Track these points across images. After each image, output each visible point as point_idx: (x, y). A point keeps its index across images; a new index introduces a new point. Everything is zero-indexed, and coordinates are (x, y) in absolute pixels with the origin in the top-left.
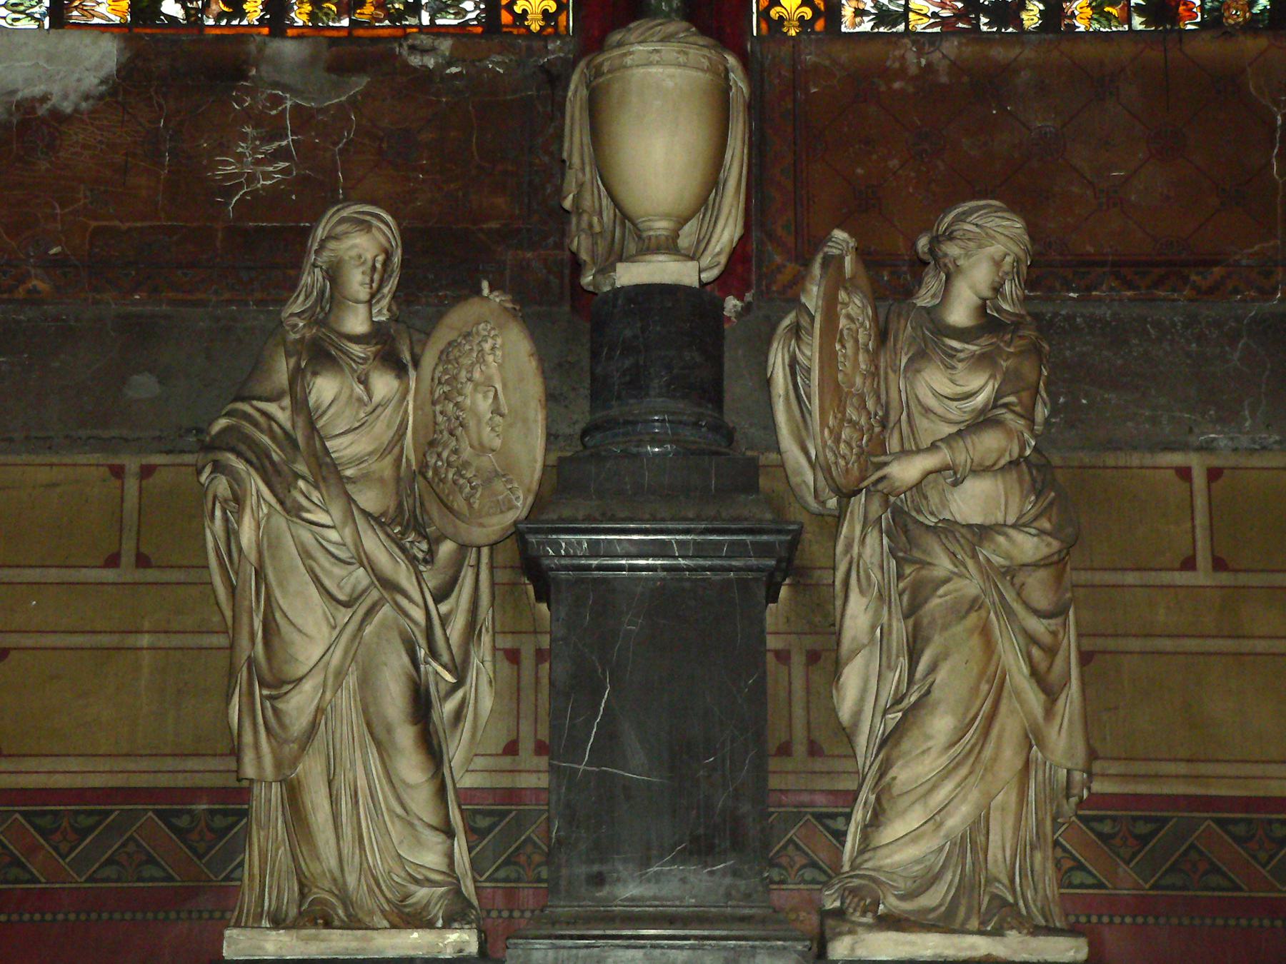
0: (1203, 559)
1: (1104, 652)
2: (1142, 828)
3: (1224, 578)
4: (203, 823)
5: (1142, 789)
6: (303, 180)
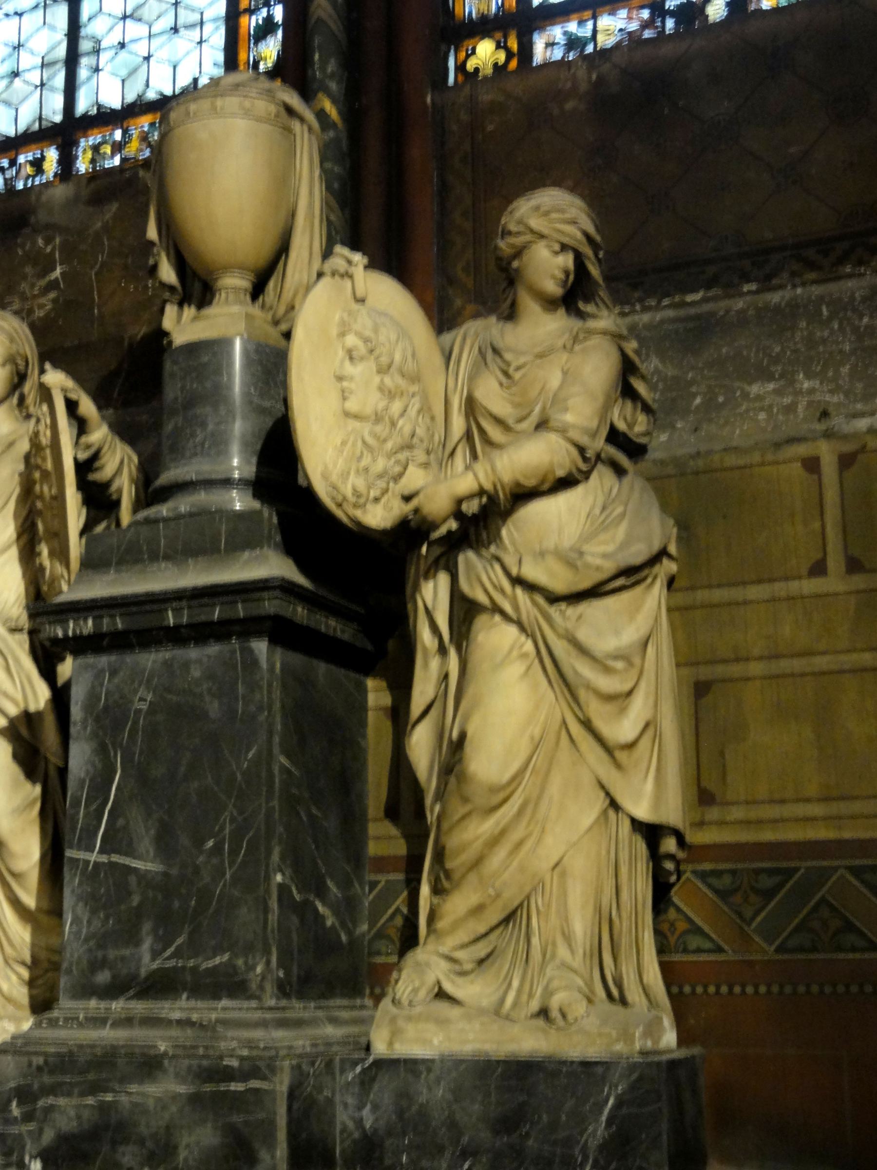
0: (835, 562)
2: (767, 882)
3: (859, 581)
5: (768, 836)
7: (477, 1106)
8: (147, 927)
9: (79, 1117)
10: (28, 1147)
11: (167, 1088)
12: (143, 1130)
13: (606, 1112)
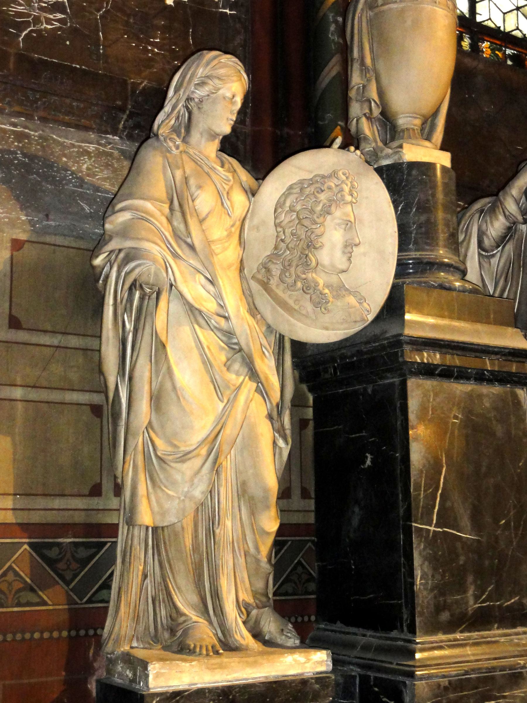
1: (102, 422)
4: (69, 555)
6: (74, 31)
8: (470, 579)
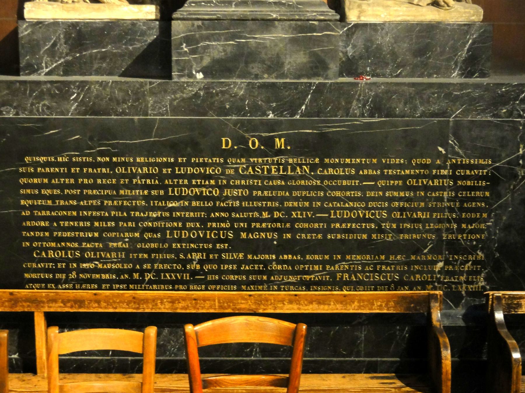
7: (406, 45)
9: (224, 51)
10: (194, 66)
11: (278, 36)
12: (263, 56)
13: (467, 46)
